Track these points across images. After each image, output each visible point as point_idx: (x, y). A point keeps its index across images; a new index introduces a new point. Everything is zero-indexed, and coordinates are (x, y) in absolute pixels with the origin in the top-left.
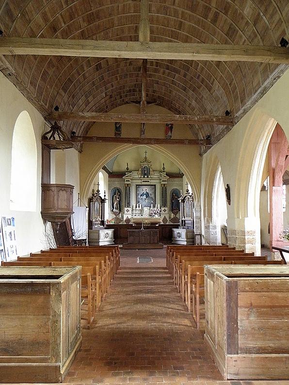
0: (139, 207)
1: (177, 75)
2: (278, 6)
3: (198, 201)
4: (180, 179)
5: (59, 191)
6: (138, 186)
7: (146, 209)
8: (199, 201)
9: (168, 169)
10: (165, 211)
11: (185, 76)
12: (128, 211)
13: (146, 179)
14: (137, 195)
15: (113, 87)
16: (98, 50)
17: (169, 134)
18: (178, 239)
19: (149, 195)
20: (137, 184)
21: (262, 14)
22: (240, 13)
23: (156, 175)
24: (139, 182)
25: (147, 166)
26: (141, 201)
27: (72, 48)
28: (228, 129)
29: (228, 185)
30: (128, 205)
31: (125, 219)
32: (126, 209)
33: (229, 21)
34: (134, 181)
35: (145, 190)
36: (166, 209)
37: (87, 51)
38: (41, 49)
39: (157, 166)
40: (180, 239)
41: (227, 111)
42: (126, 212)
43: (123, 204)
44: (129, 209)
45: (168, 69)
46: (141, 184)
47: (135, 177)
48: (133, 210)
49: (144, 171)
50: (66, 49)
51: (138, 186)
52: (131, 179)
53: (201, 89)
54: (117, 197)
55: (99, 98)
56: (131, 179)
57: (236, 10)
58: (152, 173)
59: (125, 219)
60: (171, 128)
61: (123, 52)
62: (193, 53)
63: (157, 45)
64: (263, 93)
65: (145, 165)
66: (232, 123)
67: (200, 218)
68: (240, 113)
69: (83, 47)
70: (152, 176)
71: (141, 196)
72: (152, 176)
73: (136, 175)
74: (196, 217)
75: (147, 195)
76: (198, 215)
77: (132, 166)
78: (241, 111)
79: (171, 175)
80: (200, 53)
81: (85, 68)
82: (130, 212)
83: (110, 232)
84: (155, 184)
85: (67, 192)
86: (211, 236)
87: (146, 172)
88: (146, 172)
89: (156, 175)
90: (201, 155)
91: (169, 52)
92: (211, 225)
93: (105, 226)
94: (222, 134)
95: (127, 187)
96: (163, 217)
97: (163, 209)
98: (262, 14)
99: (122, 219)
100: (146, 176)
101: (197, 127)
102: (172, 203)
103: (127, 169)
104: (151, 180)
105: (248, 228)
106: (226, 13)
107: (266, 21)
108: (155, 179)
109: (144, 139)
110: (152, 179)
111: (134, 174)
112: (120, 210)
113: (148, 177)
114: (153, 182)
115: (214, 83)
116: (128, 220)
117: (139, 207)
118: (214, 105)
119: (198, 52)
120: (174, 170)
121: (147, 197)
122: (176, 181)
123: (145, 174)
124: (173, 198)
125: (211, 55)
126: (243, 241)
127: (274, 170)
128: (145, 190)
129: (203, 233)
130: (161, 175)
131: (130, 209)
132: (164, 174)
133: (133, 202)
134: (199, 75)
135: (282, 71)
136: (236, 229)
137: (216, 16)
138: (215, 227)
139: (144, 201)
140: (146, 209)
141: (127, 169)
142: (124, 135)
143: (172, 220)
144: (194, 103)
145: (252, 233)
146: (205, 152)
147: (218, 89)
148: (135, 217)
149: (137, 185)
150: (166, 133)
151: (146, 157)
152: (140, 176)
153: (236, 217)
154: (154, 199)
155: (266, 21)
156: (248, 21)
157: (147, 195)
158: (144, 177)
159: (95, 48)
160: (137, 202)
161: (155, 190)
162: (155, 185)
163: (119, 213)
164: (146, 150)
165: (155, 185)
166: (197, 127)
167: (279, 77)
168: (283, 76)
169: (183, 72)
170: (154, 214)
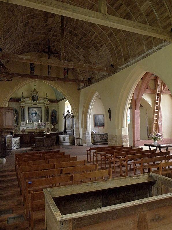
0: (31, 121)
1: (75, 38)
2: (169, 8)
3: (77, 118)
4: (56, 104)
5: (6, 112)
6: (29, 108)
7: (36, 123)
8: (78, 118)
9: (49, 97)
10: (48, 124)
11: (81, 39)
12: (23, 124)
13: (35, 103)
14: (29, 114)
15: (28, 39)
16: (76, 13)
17: (67, 75)
18: (63, 141)
19: (37, 114)
20: (29, 106)
21: (154, 11)
22: (138, 7)
23: (42, 101)
24: (30, 105)
25: (36, 94)
26: (32, 118)
27: (58, 8)
28: (109, 75)
29: (109, 109)
30: (24, 120)
31: (21, 129)
32: (22, 123)
33: (128, 10)
34: (27, 104)
35: (34, 110)
36: (49, 122)
37: (68, 12)
38: (34, 3)
39: (42, 94)
40: (65, 142)
41: (112, 64)
42: (22, 125)
43: (20, 119)
44: (24, 123)
45: (70, 33)
46: (31, 106)
47: (28, 101)
48: (26, 124)
49: (34, 98)
50: (54, 7)
51: (29, 108)
52: (25, 103)
53: (91, 49)
54: (15, 115)
55: (17, 46)
56: (25, 103)
57: (136, 5)
58: (39, 99)
59: (21, 129)
60: (67, 72)
61: (92, 18)
62: (132, 27)
63: (112, 17)
64: (145, 57)
65: (35, 94)
66: (114, 72)
67: (79, 128)
68: (123, 66)
69: (65, 8)
70: (39, 101)
71: (32, 114)
72: (39, 101)
73: (28, 100)
74: (76, 128)
75: (36, 114)
76: (77, 126)
77: (25, 95)
78: (125, 65)
79: (52, 101)
80: (135, 28)
81: (19, 23)
82: (25, 125)
83: (18, 139)
84: (41, 106)
85: (11, 113)
86: (87, 139)
87: (35, 99)
88: (35, 99)
89: (42, 101)
90: (79, 89)
91: (119, 24)
92: (86, 132)
93: (13, 136)
94: (104, 77)
95: (22, 108)
96: (47, 127)
97: (47, 122)
98: (154, 11)
99: (19, 130)
100: (35, 101)
101: (79, 72)
102: (52, 119)
103: (22, 96)
104: (38, 103)
105: (124, 134)
106: (128, 6)
107: (157, 15)
108: (40, 103)
109: (50, 77)
110: (39, 103)
111: (26, 100)
112: (17, 124)
113: (36, 102)
114: (39, 105)
115: (103, 47)
116: (23, 131)
117: (31, 121)
118: (98, 60)
119: (134, 27)
120: (53, 97)
121: (36, 115)
122: (54, 105)
123: (34, 100)
124: (52, 116)
125: (140, 30)
126: (121, 142)
127: (136, 101)
128: (34, 110)
129: (81, 137)
130: (45, 101)
131: (25, 123)
132: (47, 100)
133: (27, 119)
134: (92, 40)
135: (164, 46)
136: (117, 135)
137: (120, 5)
138: (89, 133)
139: (34, 117)
140: (36, 123)
141: (22, 96)
142: (37, 73)
143: (53, 130)
144: (81, 57)
145: (126, 137)
146: (83, 88)
147: (104, 50)
148: (28, 128)
149: (29, 107)
150: (65, 74)
151: (35, 89)
152: (31, 101)
153: (116, 127)
154: (40, 116)
155: (157, 15)
156: (142, 13)
157: (36, 114)
158: (34, 102)
159: (74, 11)
160: (29, 118)
161: (41, 110)
162: (41, 107)
163: (17, 126)
164: (34, 84)
165: (41, 107)
166: (79, 72)
167: (160, 49)
168: (163, 49)
169: (80, 36)
170: (41, 126)
